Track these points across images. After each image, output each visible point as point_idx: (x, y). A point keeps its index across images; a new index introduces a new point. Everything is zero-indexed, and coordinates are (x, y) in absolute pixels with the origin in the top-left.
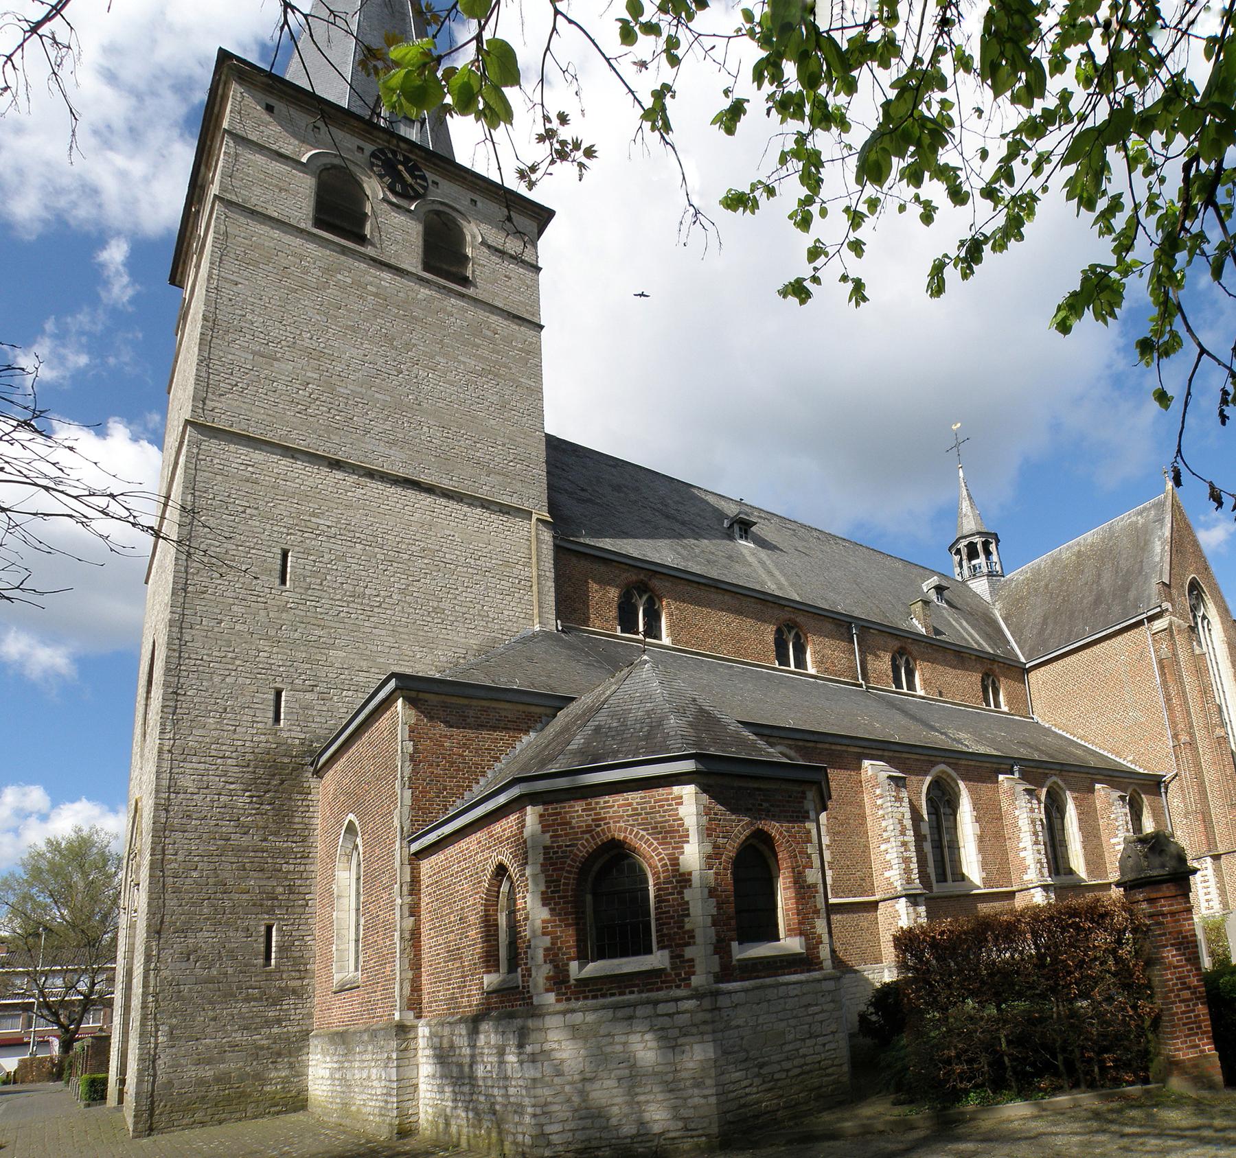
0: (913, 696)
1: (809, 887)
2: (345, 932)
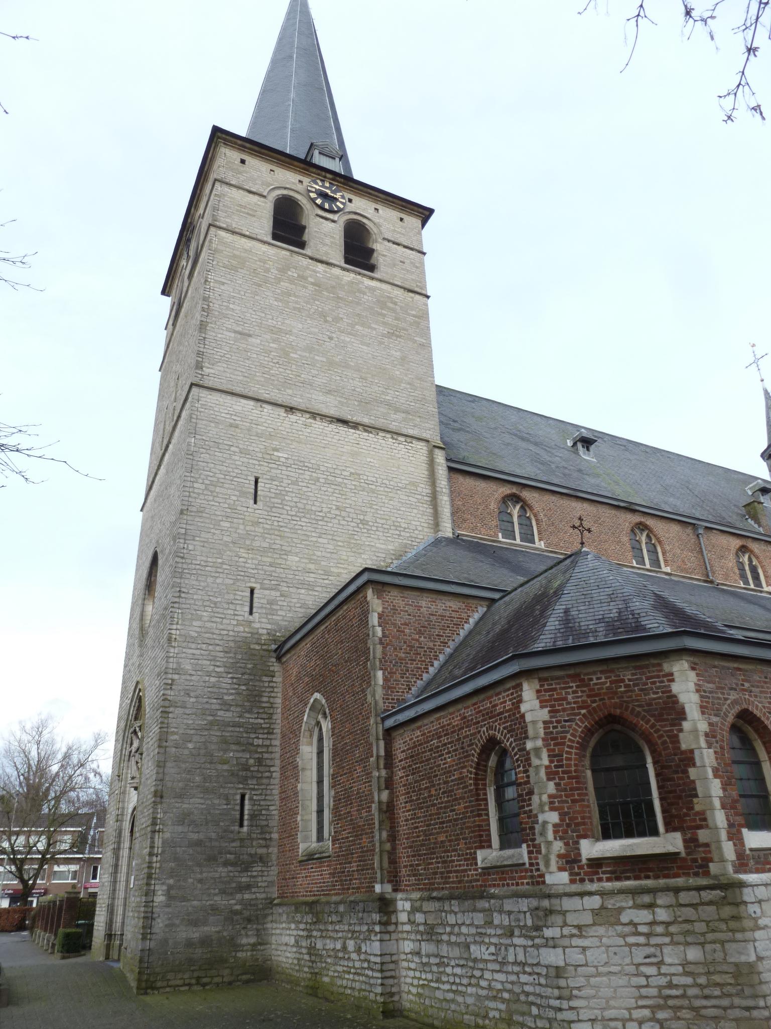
0: (761, 592)
2: (308, 803)
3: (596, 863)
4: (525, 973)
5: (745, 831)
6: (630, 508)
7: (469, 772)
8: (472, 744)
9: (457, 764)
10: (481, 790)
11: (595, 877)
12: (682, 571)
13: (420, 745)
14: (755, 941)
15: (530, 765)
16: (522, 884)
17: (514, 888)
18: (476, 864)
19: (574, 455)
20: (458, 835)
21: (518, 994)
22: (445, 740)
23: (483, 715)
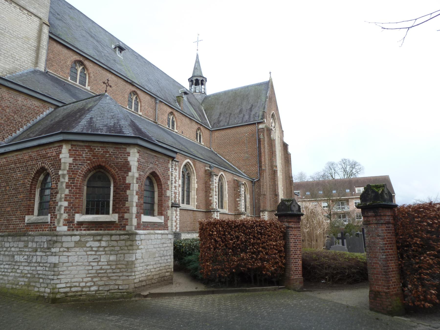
1: (167, 197)
3: (80, 224)
4: (39, 266)
5: (142, 215)
6: (132, 84)
7: (28, 182)
8: (32, 169)
9: (23, 177)
10: (33, 189)
11: (79, 229)
12: (146, 115)
13: (4, 166)
14: (136, 253)
15: (59, 181)
16: (45, 230)
17: (41, 232)
18: (24, 221)
19: (113, 52)
20: (17, 208)
21: (35, 275)
22: (18, 165)
23: (41, 157)
